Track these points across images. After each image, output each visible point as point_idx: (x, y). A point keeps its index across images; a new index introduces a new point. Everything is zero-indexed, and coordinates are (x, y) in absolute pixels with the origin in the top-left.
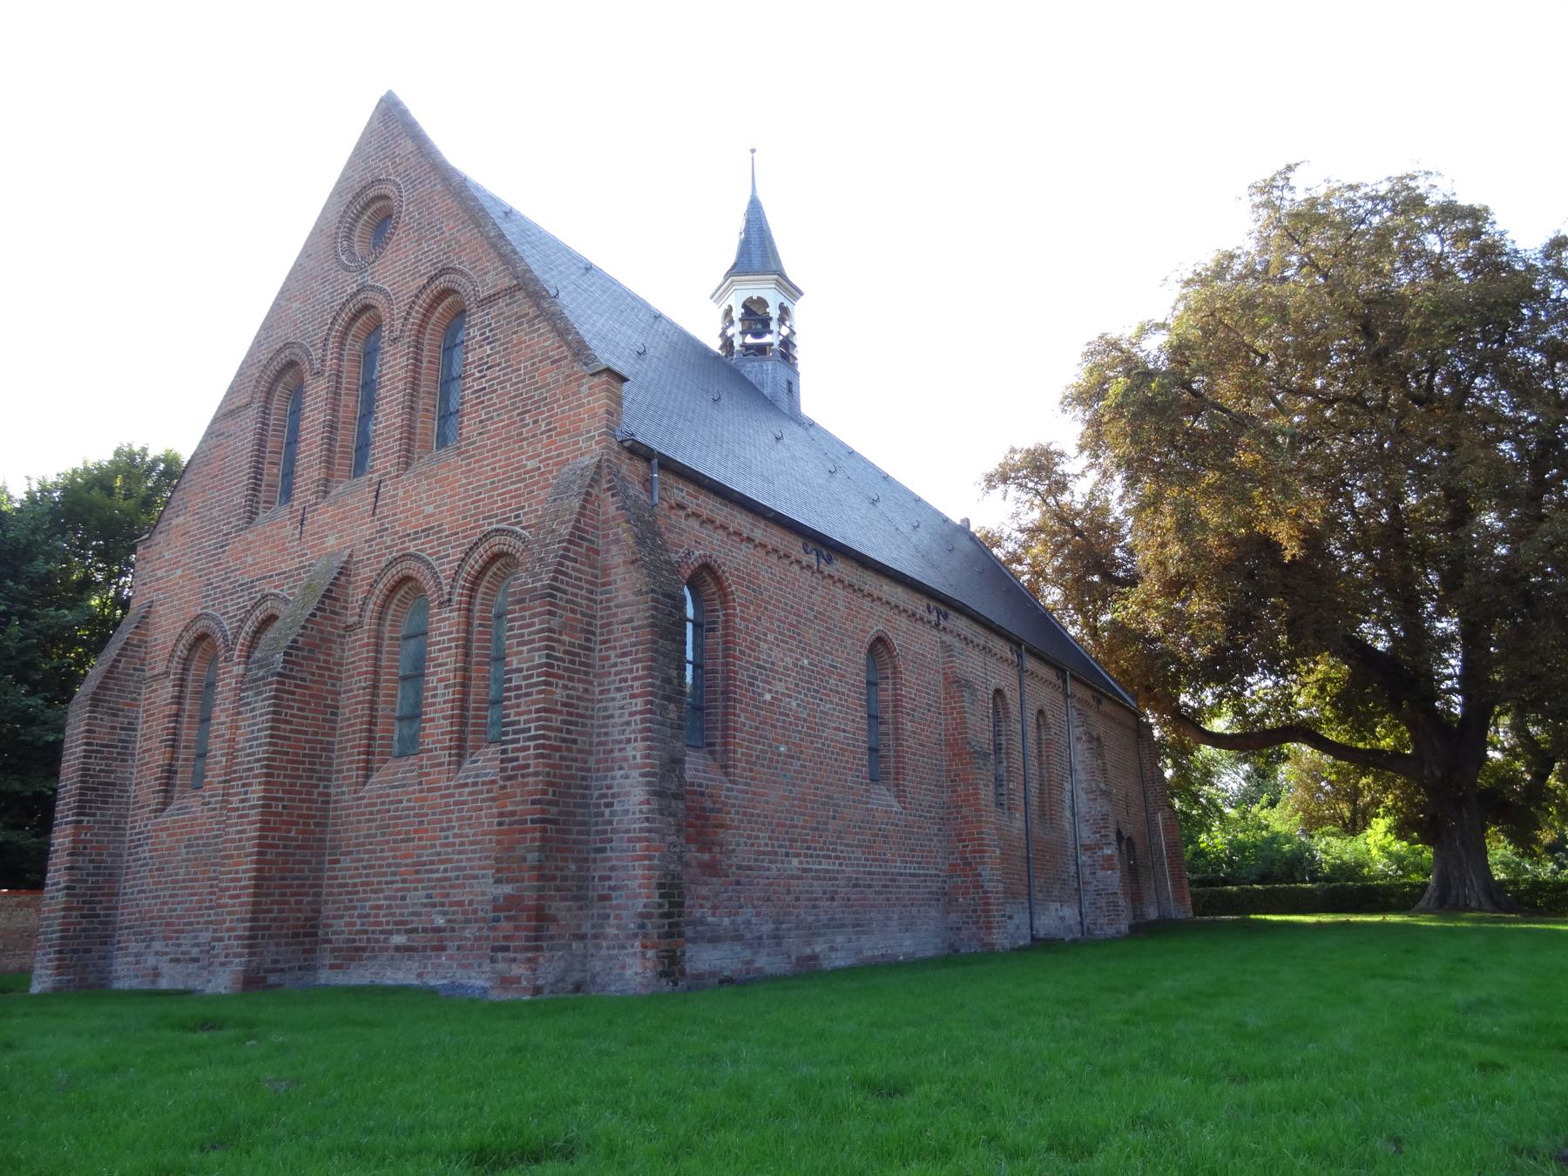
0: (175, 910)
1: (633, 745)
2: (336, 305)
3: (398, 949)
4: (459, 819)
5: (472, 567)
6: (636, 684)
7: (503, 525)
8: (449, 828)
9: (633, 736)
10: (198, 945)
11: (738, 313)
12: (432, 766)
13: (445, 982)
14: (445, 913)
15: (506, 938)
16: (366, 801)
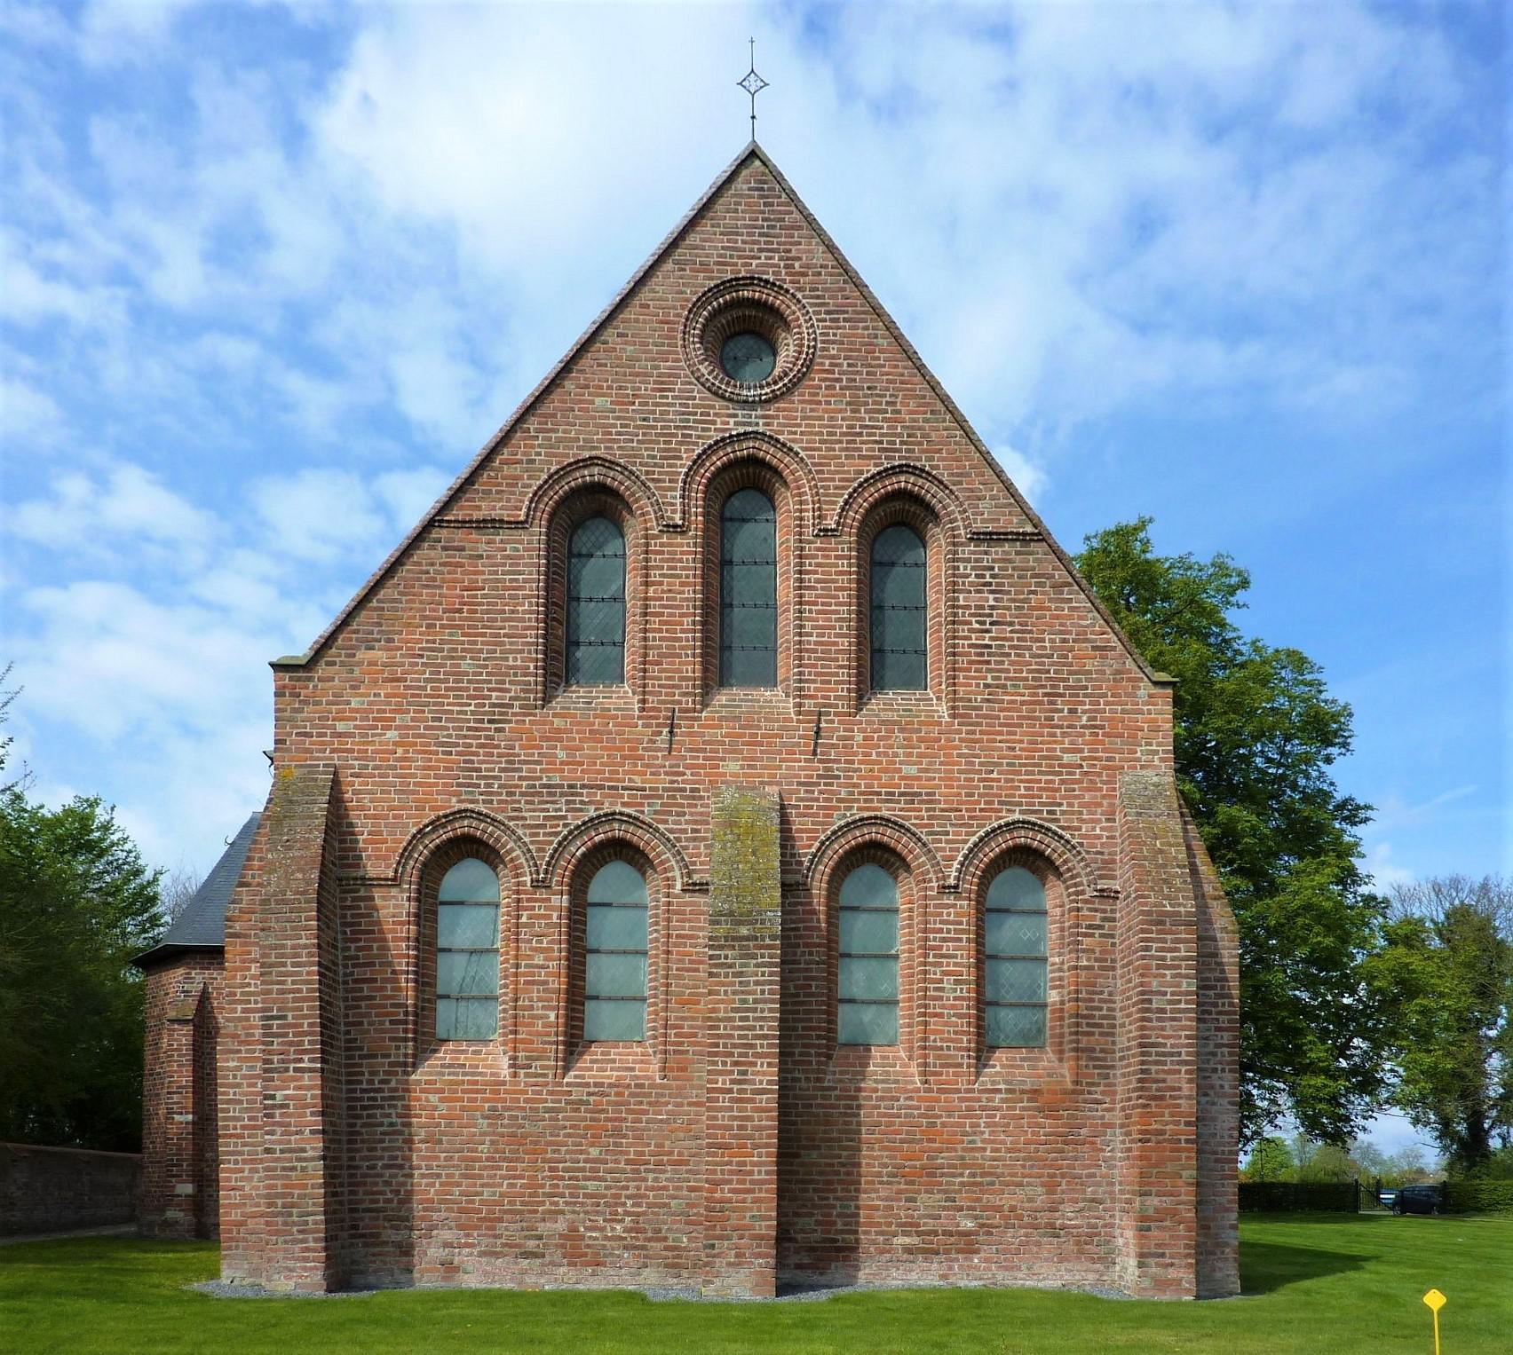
1: (1219, 1074)
3: (909, 1250)
4: (988, 1125)
6: (1132, 1027)
7: (1032, 818)
9: (1219, 1067)
14: (976, 1217)
16: (837, 1092)
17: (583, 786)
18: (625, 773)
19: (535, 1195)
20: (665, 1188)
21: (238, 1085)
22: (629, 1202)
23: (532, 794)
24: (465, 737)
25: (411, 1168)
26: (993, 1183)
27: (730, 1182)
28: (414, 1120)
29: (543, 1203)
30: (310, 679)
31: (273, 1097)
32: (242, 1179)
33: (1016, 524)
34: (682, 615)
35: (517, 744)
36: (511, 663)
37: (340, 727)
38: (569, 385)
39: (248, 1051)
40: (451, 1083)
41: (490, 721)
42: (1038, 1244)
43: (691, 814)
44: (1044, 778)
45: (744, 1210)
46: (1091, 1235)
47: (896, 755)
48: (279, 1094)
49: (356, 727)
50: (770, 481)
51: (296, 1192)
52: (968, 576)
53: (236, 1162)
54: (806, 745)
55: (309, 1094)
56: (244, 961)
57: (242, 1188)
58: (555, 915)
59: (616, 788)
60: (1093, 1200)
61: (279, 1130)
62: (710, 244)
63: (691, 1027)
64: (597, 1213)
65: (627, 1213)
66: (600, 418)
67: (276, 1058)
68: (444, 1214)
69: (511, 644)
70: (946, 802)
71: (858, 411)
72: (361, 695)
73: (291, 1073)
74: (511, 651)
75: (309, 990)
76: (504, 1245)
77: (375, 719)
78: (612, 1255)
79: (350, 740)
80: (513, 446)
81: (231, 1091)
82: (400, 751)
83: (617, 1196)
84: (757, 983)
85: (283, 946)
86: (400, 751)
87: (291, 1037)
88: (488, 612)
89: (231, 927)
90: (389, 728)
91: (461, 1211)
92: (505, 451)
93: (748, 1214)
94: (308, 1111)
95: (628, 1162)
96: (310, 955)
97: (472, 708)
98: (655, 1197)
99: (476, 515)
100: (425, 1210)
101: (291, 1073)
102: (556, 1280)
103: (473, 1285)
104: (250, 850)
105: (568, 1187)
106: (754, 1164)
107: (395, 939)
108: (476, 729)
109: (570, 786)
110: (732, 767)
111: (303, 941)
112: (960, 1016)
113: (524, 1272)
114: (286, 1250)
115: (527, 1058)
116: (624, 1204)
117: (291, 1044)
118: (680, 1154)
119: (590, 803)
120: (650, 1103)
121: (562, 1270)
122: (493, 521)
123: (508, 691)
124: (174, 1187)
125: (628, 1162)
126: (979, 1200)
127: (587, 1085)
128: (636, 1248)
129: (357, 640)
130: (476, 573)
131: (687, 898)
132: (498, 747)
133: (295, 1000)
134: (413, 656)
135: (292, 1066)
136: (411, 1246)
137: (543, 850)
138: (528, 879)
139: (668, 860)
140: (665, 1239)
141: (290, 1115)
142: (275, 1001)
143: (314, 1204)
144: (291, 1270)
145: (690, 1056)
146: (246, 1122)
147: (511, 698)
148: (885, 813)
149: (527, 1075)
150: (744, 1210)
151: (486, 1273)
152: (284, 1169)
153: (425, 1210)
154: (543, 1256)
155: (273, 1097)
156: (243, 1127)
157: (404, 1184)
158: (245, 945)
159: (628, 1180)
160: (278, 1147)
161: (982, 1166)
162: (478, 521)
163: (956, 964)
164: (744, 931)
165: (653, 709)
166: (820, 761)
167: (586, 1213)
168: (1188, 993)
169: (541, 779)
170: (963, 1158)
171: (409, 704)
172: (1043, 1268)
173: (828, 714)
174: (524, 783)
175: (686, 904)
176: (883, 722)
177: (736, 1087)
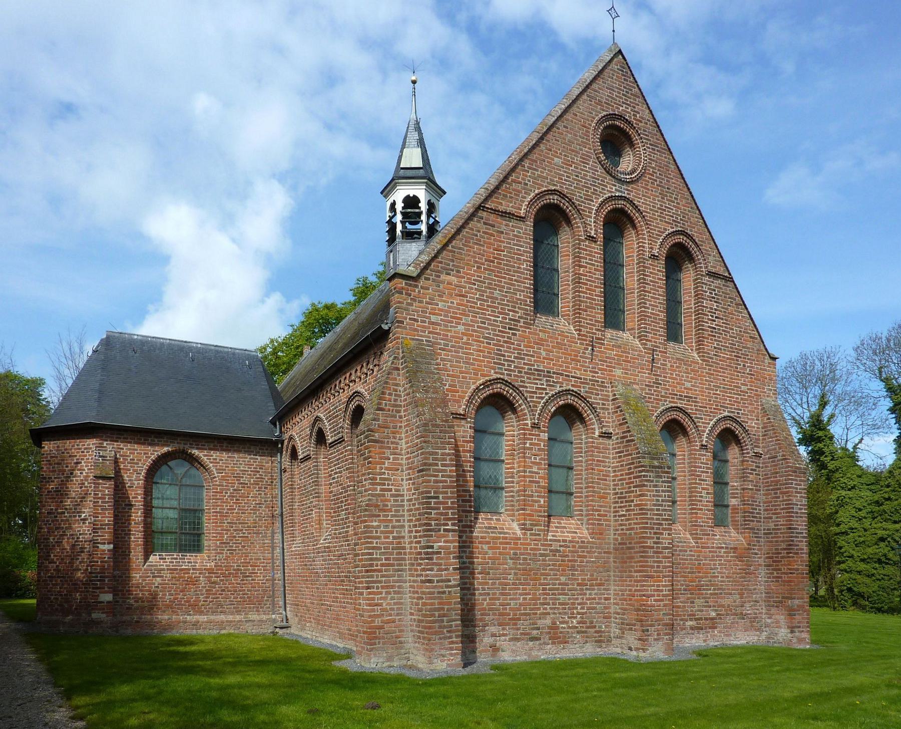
3: (692, 628)
4: (720, 565)
8: (715, 569)
11: (399, 206)
12: (703, 535)
13: (716, 644)
14: (716, 611)
15: (799, 622)
17: (554, 373)
18: (573, 368)
19: (535, 604)
20: (594, 599)
21: (379, 538)
22: (579, 607)
23: (530, 374)
24: (498, 335)
25: (474, 589)
26: (721, 594)
27: (653, 596)
28: (475, 560)
29: (539, 609)
30: (416, 286)
31: (432, 547)
32: (381, 598)
33: (721, 270)
34: (596, 287)
35: (522, 343)
36: (518, 297)
37: (433, 318)
38: (542, 147)
39: (384, 516)
40: (494, 538)
41: (510, 329)
42: (737, 623)
43: (602, 395)
44: (735, 396)
45: (660, 610)
46: (755, 618)
47: (683, 376)
48: (436, 545)
49: (441, 320)
50: (625, 222)
51: (446, 607)
52: (706, 292)
53: (378, 588)
54: (648, 366)
55: (452, 545)
56: (381, 458)
57: (380, 605)
58: (542, 444)
59: (568, 376)
60: (756, 601)
61: (435, 568)
62: (602, 91)
63: (605, 511)
64: (565, 613)
65: (578, 613)
66: (557, 169)
67: (433, 523)
68: (491, 617)
69: (518, 286)
70: (702, 403)
71: (664, 199)
72: (444, 301)
73: (442, 532)
74: (519, 291)
75: (451, 482)
76: (522, 634)
77: (452, 317)
78: (572, 637)
79: (439, 327)
80: (517, 173)
81: (375, 541)
82: (465, 338)
83: (573, 604)
84: (663, 491)
85: (437, 453)
86: (465, 338)
87: (442, 510)
88: (507, 265)
89: (373, 436)
90: (459, 324)
91: (501, 614)
92: (513, 174)
93: (662, 613)
94: (451, 556)
95: (579, 584)
96: (451, 460)
97: (500, 319)
98: (591, 603)
99: (501, 208)
100: (482, 615)
101: (442, 532)
102: (546, 653)
103: (506, 658)
104: (384, 387)
105: (551, 599)
106: (663, 586)
107: (464, 451)
108: (502, 332)
109: (548, 372)
110: (618, 372)
111: (447, 451)
112: (709, 510)
113: (531, 649)
114: (441, 643)
115: (531, 525)
116: (577, 608)
117: (442, 514)
118: (601, 580)
119: (557, 382)
120: (588, 552)
121: (549, 646)
122: (509, 213)
123: (517, 312)
124: (98, 596)
125: (579, 584)
126: (717, 602)
127: (559, 541)
128: (583, 632)
129: (441, 268)
130: (500, 241)
131: (601, 440)
132: (513, 344)
133: (444, 487)
134: (470, 283)
135: (442, 528)
136: (475, 637)
137: (536, 407)
138: (529, 422)
139: (524, 409)
140: (595, 627)
141: (442, 559)
142: (432, 487)
143: (456, 614)
144: (444, 656)
145: (604, 527)
146: (384, 561)
147: (519, 317)
148: (679, 405)
149: (531, 534)
150: (660, 610)
151: (513, 651)
152: (439, 593)
153: (482, 615)
154: (540, 639)
155: (432, 547)
156: (382, 565)
157: (471, 599)
158: (381, 448)
159: (578, 594)
160: (435, 579)
161: (717, 585)
162: (502, 212)
163: (707, 485)
164: (656, 463)
165: (584, 335)
166: (654, 375)
167: (560, 613)
168: (805, 505)
169: (534, 366)
170: (710, 581)
171: (469, 311)
172: (740, 634)
173: (657, 351)
174: (526, 367)
175: (600, 444)
176: (678, 359)
177: (655, 545)
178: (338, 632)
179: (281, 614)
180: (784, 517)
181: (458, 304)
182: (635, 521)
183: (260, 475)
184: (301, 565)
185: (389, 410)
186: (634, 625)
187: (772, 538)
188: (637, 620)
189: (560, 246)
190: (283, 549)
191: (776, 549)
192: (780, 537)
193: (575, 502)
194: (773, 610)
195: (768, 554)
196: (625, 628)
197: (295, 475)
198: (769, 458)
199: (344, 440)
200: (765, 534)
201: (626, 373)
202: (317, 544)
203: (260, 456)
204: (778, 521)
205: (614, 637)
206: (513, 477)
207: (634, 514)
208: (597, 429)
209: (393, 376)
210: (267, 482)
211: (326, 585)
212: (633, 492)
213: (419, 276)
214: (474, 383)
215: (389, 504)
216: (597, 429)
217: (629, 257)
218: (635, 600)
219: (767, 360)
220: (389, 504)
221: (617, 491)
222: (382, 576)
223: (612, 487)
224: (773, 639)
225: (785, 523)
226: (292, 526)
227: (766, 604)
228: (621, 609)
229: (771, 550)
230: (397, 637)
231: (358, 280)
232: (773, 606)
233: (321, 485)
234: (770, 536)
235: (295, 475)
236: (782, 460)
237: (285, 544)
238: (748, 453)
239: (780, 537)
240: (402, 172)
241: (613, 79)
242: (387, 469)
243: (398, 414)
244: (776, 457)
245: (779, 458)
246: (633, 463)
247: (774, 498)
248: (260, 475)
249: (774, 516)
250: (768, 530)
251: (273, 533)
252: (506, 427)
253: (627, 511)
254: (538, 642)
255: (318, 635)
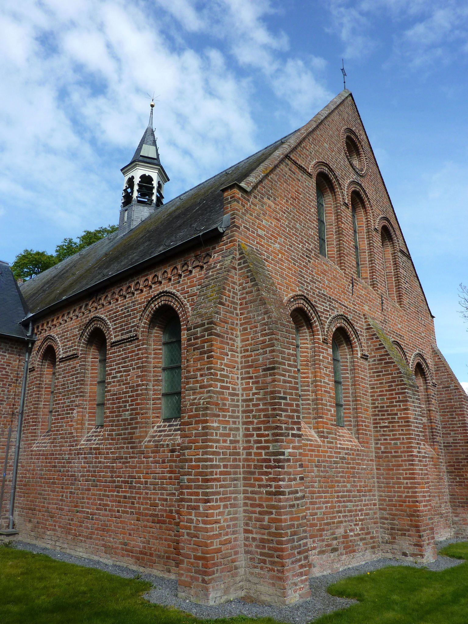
0: (316, 514)
2: (333, 167)
5: (155, 306)
10: (336, 539)
11: (137, 180)
37: (260, 232)
48: (287, 451)
82: (280, 255)
121: (344, 557)
158: (222, 342)
178: (103, 545)
179: (7, 518)
180: (461, 433)
181: (275, 226)
182: (401, 432)
183: (6, 372)
184: (46, 467)
185: (228, 306)
186: (408, 530)
187: (452, 449)
188: (411, 526)
189: (324, 206)
190: (19, 448)
191: (456, 459)
192: (460, 449)
193: (345, 413)
194: (459, 510)
195: (449, 462)
196: (395, 533)
197: (43, 374)
198: (443, 388)
199: (138, 339)
200: (444, 446)
201: (370, 310)
202: (76, 445)
203: (9, 353)
204: (455, 437)
205: (383, 542)
206: (308, 386)
207: (399, 426)
208: (359, 351)
209: (232, 274)
210: (12, 379)
211: (89, 490)
212: (396, 406)
213: (252, 191)
214: (287, 296)
215: (227, 403)
216: (359, 351)
217: (361, 227)
218: (407, 506)
219: (430, 318)
220: (227, 403)
221: (377, 405)
222: (221, 486)
223: (370, 402)
224: (462, 534)
225: (462, 438)
226: (35, 425)
227: (452, 504)
228: (390, 514)
229: (451, 459)
230: (233, 561)
231: (65, 239)
232: (459, 506)
233: (87, 385)
234: (450, 448)
235: (43, 374)
236: (455, 389)
237: (22, 443)
238: (429, 383)
239: (460, 449)
240: (141, 158)
241: (347, 110)
242: (226, 365)
243: (235, 311)
244: (449, 387)
245: (452, 388)
246: (394, 382)
247: (450, 418)
248: (6, 372)
249: (452, 433)
250: (447, 443)
251: (11, 431)
252: (301, 340)
253: (389, 423)
254: (336, 553)
255: (66, 546)
